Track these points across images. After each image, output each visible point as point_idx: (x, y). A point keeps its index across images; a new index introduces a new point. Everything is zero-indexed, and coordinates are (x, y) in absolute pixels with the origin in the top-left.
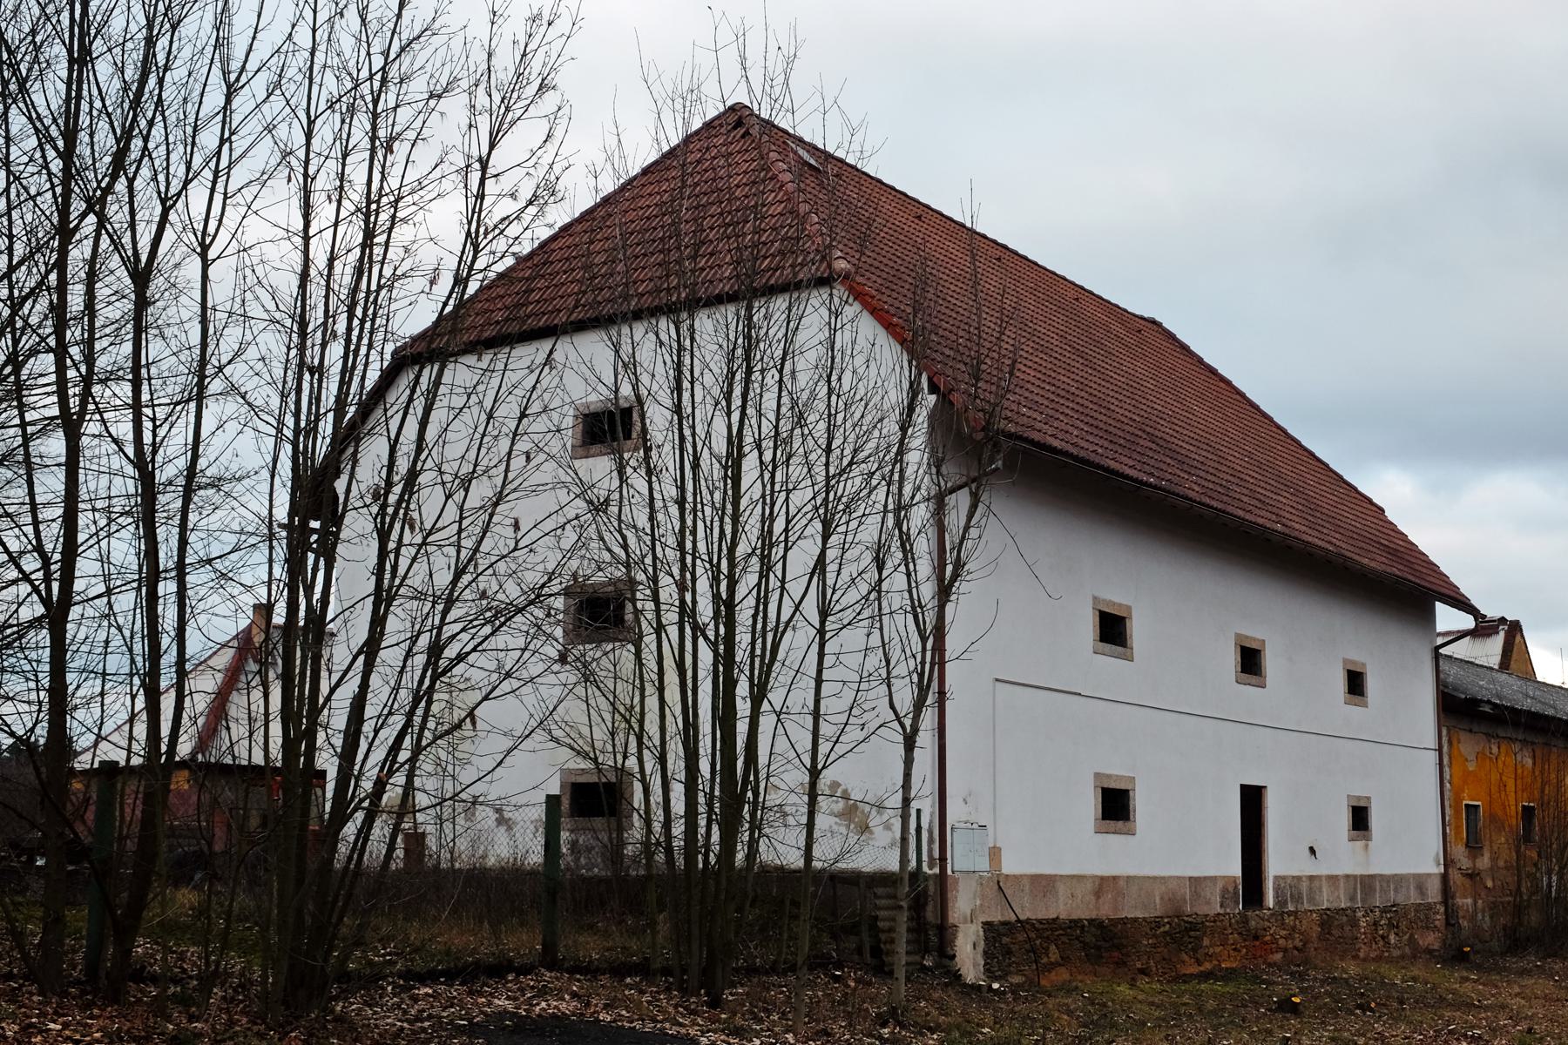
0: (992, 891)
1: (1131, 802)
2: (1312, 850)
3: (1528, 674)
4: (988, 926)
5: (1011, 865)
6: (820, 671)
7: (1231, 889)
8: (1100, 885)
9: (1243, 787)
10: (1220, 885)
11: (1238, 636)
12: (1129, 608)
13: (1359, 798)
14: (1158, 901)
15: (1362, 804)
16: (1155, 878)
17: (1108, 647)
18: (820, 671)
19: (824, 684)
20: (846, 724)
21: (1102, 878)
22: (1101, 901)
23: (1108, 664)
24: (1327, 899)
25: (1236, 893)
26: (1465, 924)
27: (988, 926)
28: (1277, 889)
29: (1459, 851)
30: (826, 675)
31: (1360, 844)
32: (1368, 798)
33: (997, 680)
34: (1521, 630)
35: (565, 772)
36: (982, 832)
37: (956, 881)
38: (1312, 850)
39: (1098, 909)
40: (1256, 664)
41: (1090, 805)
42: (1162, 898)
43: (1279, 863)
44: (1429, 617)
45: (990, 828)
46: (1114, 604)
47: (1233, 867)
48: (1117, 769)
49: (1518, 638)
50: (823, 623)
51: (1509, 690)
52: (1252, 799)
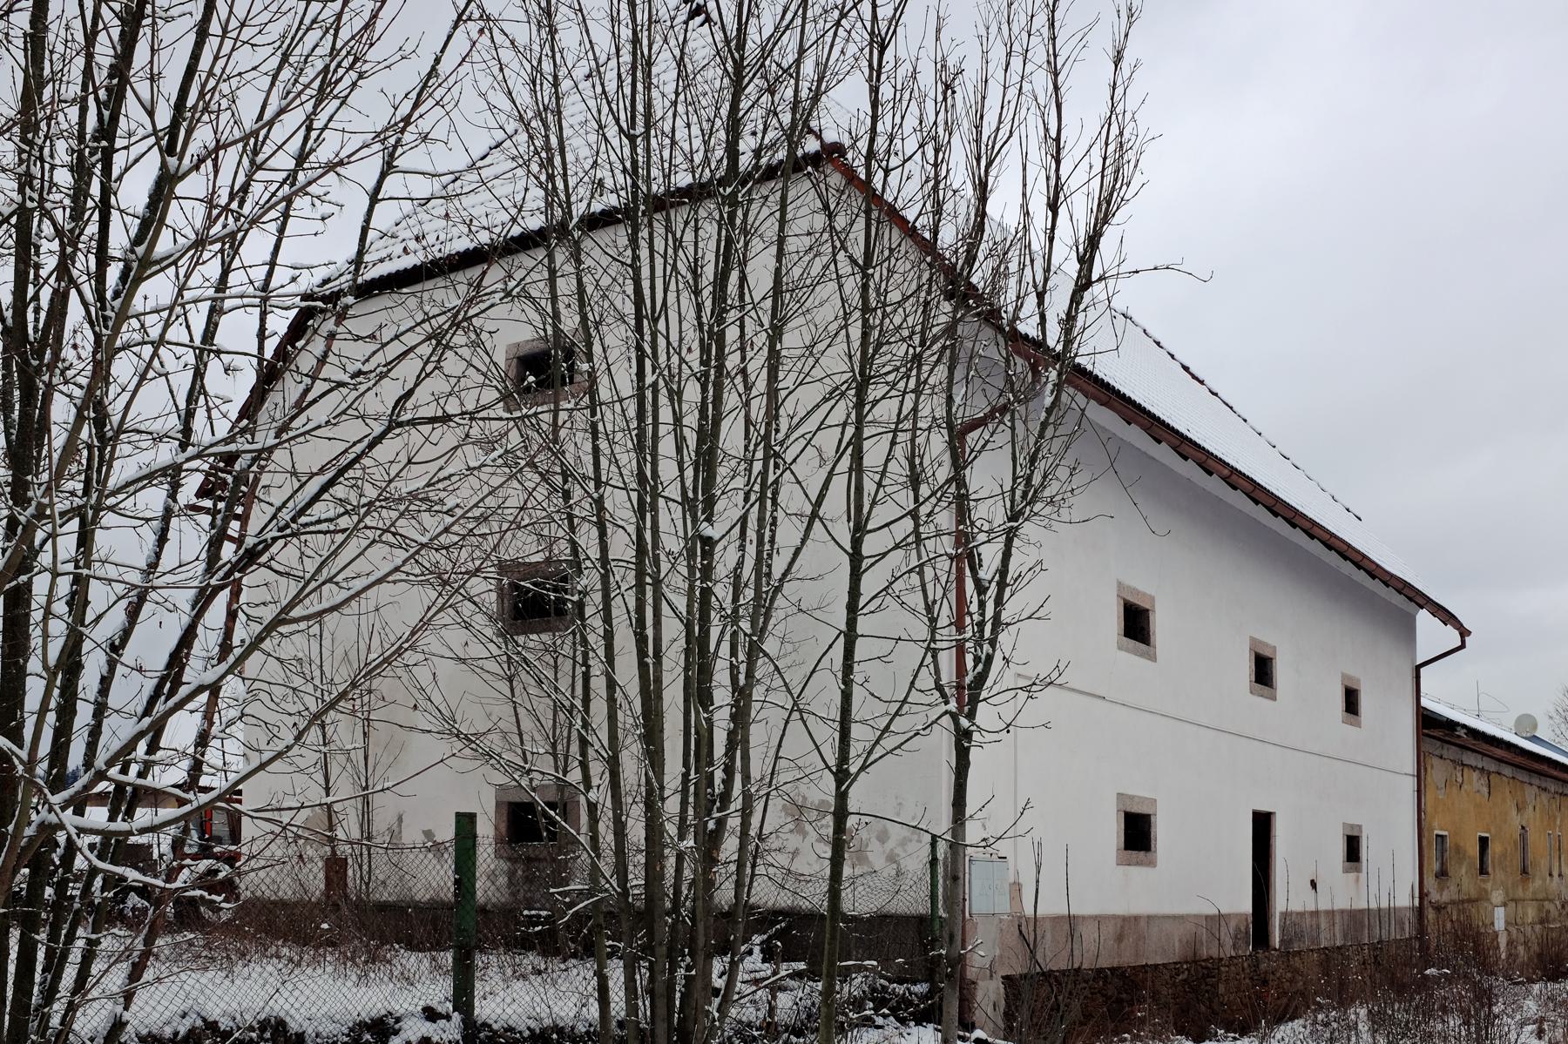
0: (1013, 939)
1: (1153, 830)
2: (1314, 884)
4: (1008, 979)
6: (851, 623)
7: (1243, 929)
9: (458, 815)
10: (1233, 924)
11: (1253, 641)
13: (1352, 826)
14: (1177, 944)
15: (1355, 834)
16: (1175, 918)
17: (1132, 643)
18: (851, 623)
19: (859, 642)
20: (904, 701)
22: (1123, 945)
23: (1128, 660)
24: (1330, 937)
25: (1247, 932)
27: (1008, 979)
28: (1283, 929)
29: (1430, 882)
30: (863, 625)
31: (1352, 875)
32: (1360, 827)
35: (501, 788)
36: (1000, 865)
37: (975, 926)
38: (1314, 884)
39: (1120, 956)
41: (1162, 832)
42: (1180, 941)
43: (1288, 897)
45: (1010, 859)
46: (1138, 592)
47: (1246, 906)
48: (1141, 789)
50: (857, 543)
52: (1262, 824)
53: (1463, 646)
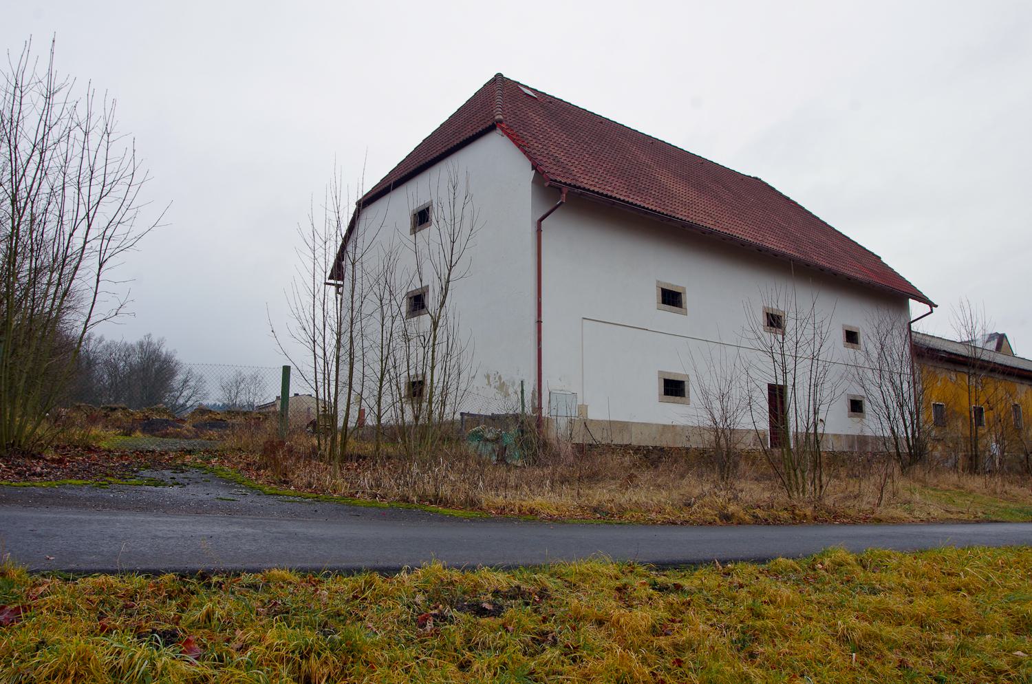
0: (583, 426)
1: (686, 388)
3: (1010, 353)
5: (593, 414)
8: (663, 429)
12: (684, 289)
21: (664, 426)
26: (994, 448)
31: (856, 419)
33: (584, 318)
34: (518, 83)
40: (679, 301)
44: (904, 307)
49: (1005, 342)
51: (1000, 359)
52: (286, 370)
53: (932, 312)
